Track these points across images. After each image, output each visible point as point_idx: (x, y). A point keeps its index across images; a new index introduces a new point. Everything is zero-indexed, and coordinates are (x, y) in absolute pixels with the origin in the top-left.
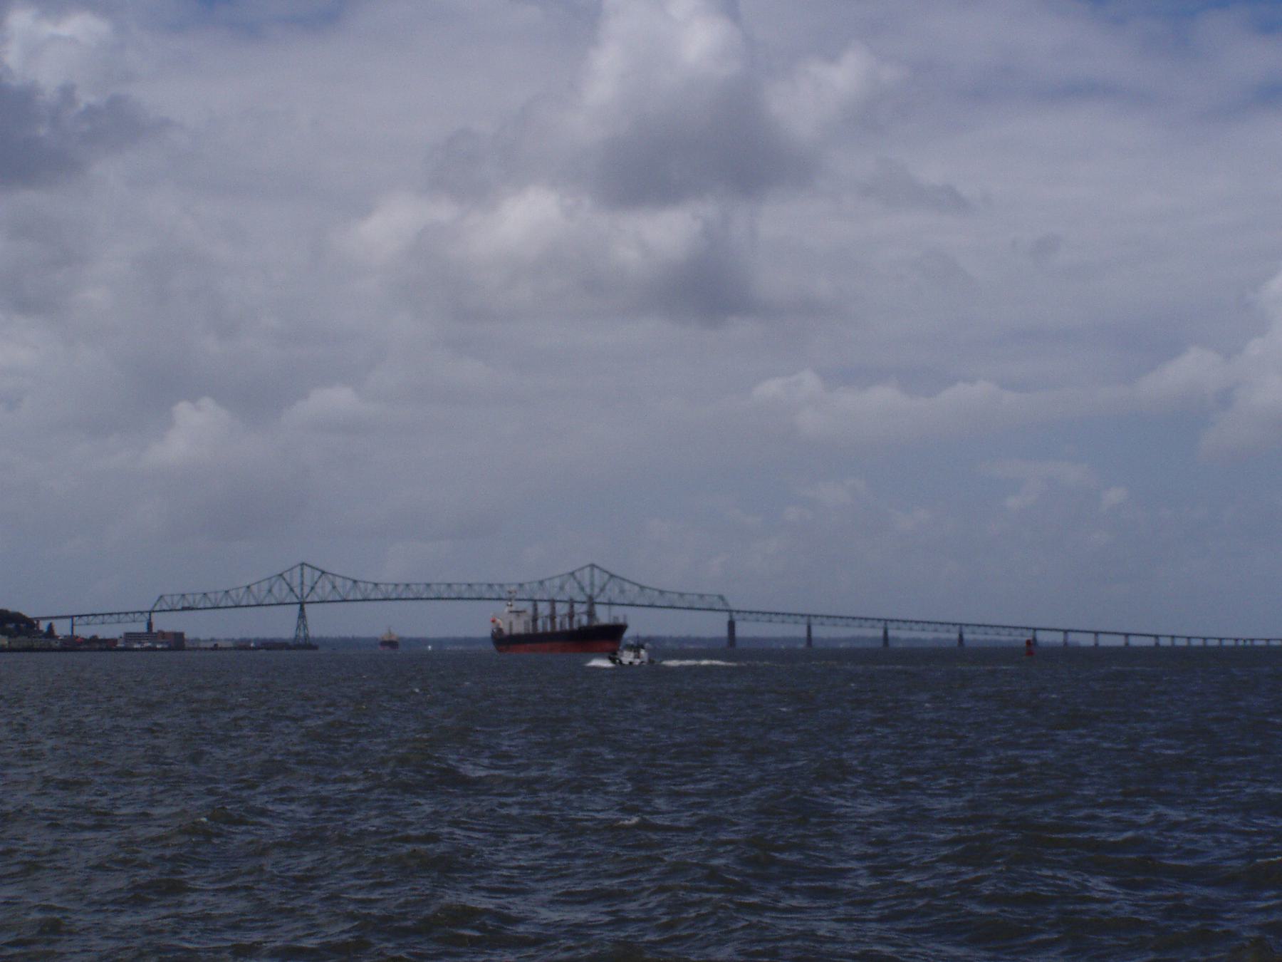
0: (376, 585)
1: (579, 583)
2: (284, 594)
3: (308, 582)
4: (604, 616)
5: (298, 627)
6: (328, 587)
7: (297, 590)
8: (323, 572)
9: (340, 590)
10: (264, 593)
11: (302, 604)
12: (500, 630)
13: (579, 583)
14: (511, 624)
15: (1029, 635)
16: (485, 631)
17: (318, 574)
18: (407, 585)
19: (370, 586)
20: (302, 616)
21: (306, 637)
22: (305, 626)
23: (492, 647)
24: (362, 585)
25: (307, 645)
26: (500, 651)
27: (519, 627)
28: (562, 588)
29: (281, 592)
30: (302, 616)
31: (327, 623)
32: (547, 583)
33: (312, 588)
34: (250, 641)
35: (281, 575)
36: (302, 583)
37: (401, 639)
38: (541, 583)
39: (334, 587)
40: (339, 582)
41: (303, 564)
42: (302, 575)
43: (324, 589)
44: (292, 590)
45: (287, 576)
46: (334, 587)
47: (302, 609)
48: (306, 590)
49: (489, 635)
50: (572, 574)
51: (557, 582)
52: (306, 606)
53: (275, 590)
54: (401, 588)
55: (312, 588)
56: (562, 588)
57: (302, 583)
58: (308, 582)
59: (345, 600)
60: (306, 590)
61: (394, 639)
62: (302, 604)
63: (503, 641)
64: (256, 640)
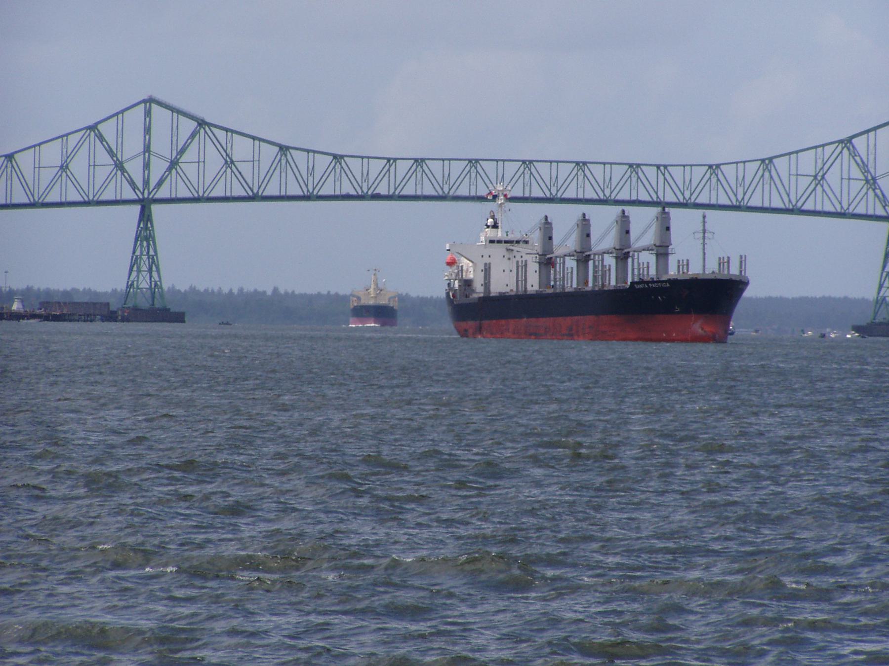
0: (337, 158)
1: (864, 167)
2: (102, 174)
3: (162, 145)
4: (694, 254)
5: (135, 262)
6: (214, 160)
7: (135, 169)
8: (202, 123)
9: (246, 169)
10: (47, 176)
11: (145, 205)
12: (467, 284)
13: (864, 167)
14: (487, 270)
15: (384, 328)
16: (434, 285)
17: (187, 126)
18: (419, 161)
19: (323, 162)
20: (145, 233)
21: (155, 289)
22: (153, 262)
23: (446, 326)
24: (300, 158)
25: (158, 311)
26: (464, 333)
27: (503, 283)
28: (819, 178)
29: (91, 170)
30: (145, 233)
31: (210, 254)
32: (781, 164)
33: (174, 164)
34: (11, 295)
35: (93, 128)
36: (147, 149)
37: (402, 298)
38: (767, 162)
39: (229, 162)
40: (241, 149)
41: (151, 100)
42: (147, 130)
43: (203, 167)
44: (119, 166)
45: (108, 130)
46: (229, 162)
47: (145, 216)
48: (158, 168)
49: (440, 292)
50: (847, 142)
51: (808, 163)
52: (156, 210)
53: (79, 166)
54: (403, 167)
55: (174, 164)
56: (819, 178)
57: (147, 149)
58: (162, 145)
59: (253, 198)
60: (158, 168)
61: (383, 301)
62: (145, 205)
63: (477, 311)
64: (26, 294)
